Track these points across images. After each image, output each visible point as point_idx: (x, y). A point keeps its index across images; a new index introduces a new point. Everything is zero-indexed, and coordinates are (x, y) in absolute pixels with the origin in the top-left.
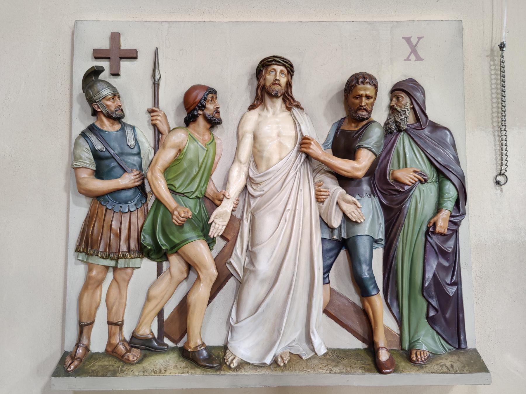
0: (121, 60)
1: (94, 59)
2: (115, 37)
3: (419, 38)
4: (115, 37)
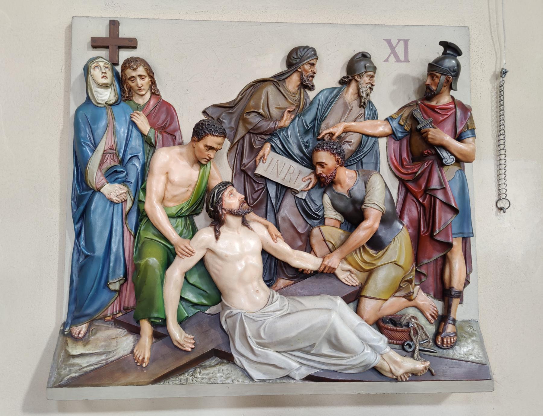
0: (120, 49)
2: (114, 25)
3: (387, 60)
4: (114, 25)
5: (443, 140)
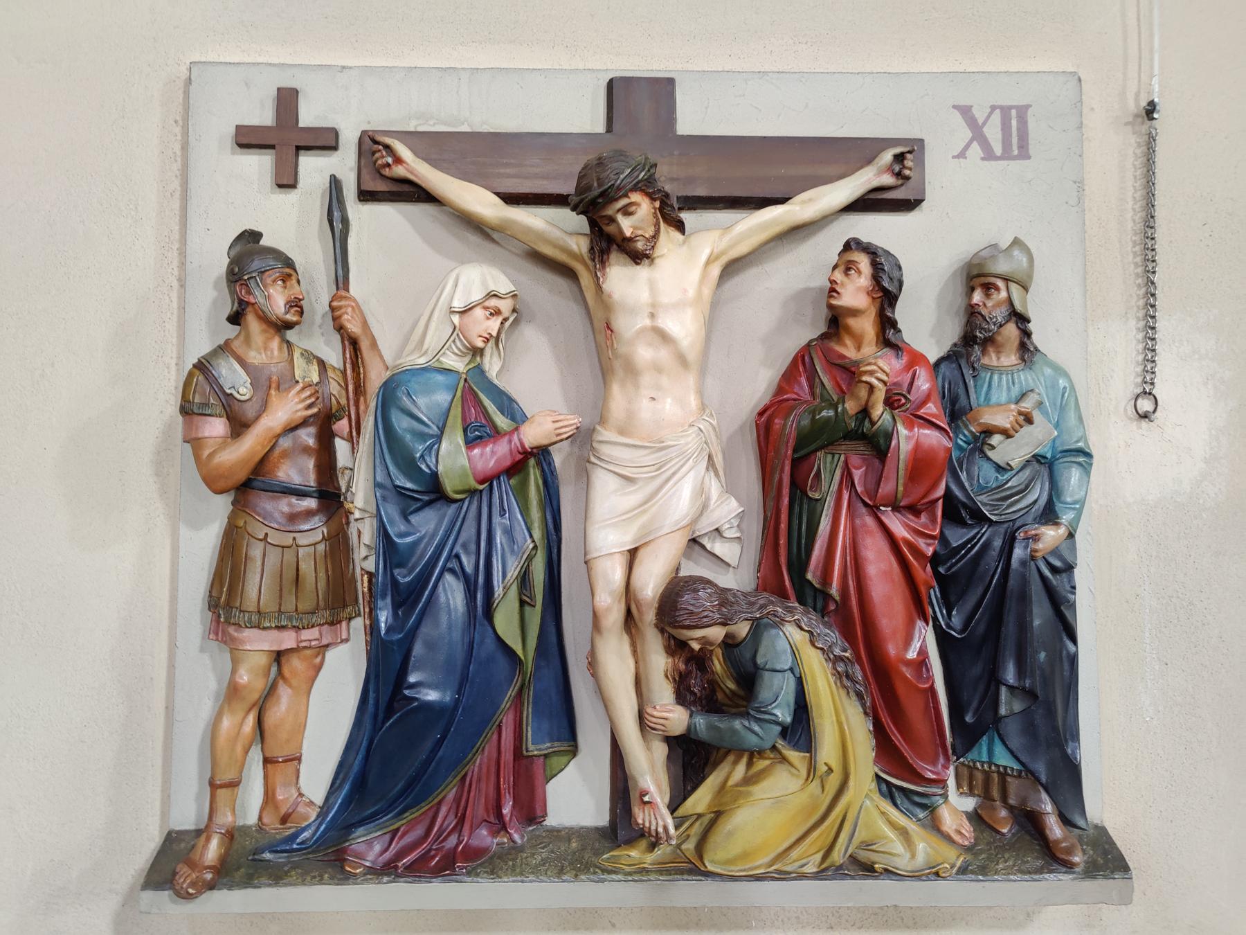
0: (302, 152)
1: (238, 149)
2: (287, 100)
3: (962, 155)
4: (287, 100)
5: (463, 614)
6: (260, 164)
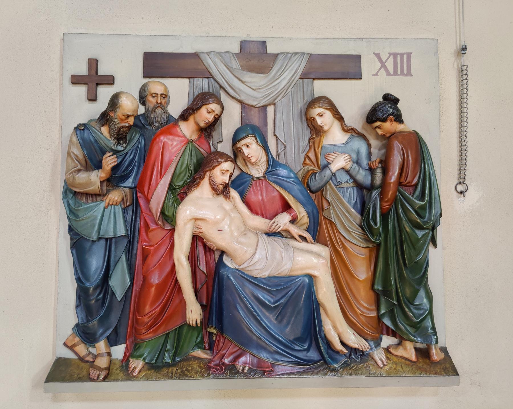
2: (93, 63)
3: (376, 75)
6: (82, 90)
